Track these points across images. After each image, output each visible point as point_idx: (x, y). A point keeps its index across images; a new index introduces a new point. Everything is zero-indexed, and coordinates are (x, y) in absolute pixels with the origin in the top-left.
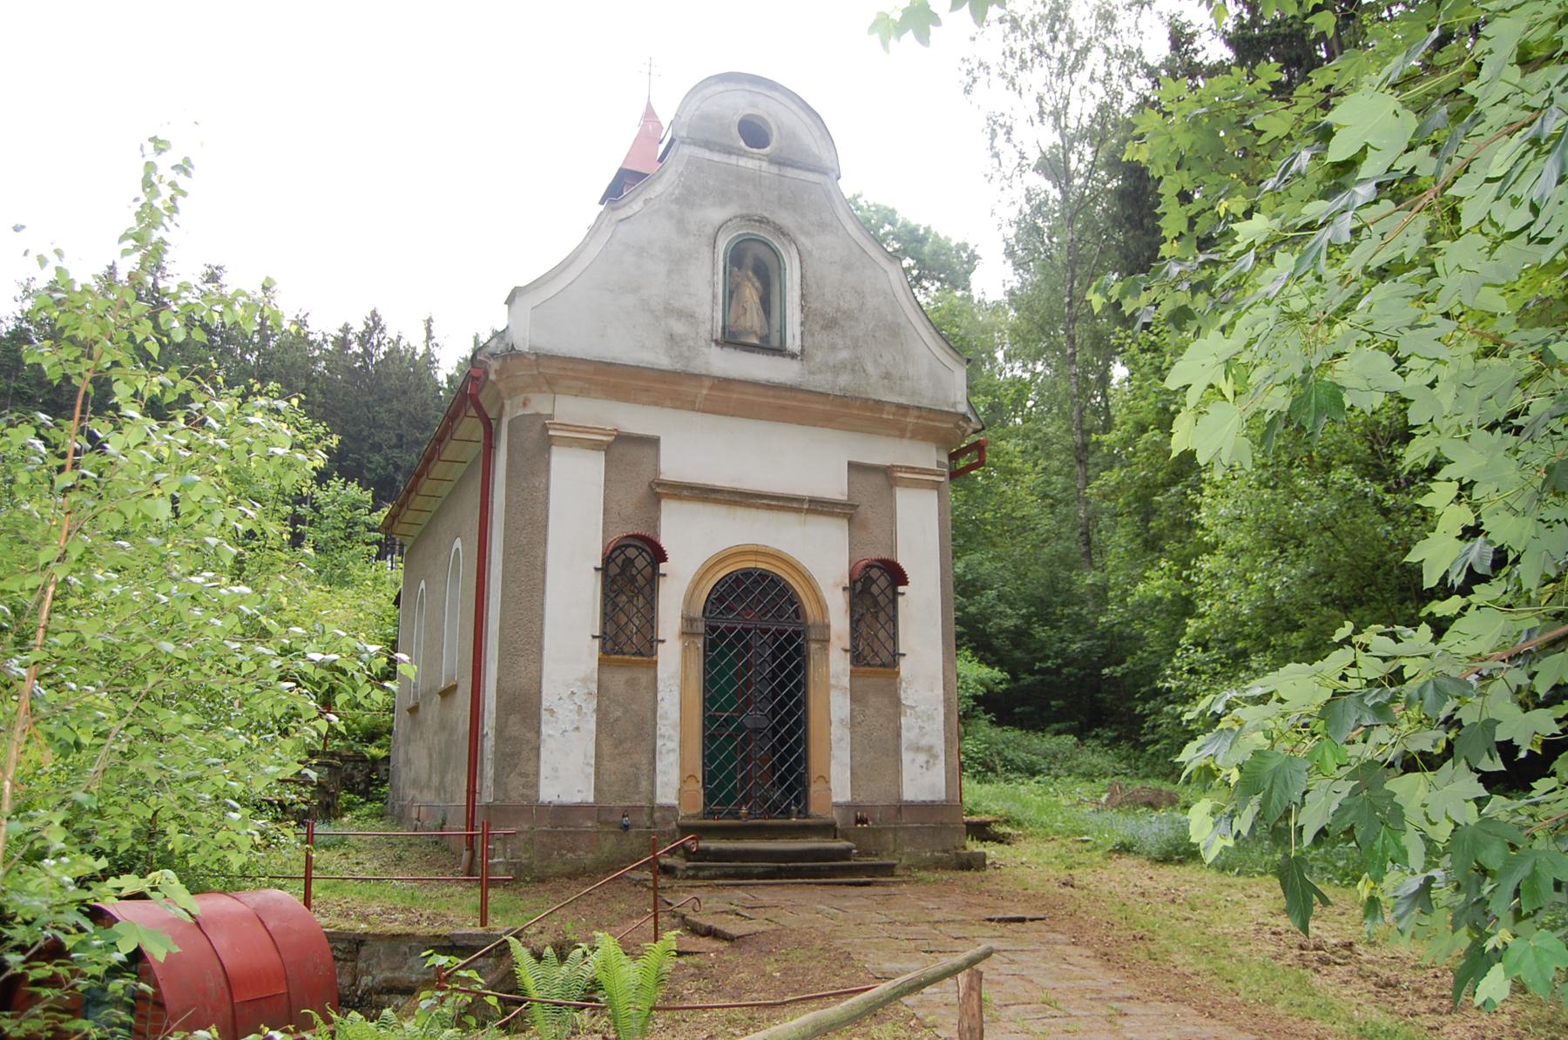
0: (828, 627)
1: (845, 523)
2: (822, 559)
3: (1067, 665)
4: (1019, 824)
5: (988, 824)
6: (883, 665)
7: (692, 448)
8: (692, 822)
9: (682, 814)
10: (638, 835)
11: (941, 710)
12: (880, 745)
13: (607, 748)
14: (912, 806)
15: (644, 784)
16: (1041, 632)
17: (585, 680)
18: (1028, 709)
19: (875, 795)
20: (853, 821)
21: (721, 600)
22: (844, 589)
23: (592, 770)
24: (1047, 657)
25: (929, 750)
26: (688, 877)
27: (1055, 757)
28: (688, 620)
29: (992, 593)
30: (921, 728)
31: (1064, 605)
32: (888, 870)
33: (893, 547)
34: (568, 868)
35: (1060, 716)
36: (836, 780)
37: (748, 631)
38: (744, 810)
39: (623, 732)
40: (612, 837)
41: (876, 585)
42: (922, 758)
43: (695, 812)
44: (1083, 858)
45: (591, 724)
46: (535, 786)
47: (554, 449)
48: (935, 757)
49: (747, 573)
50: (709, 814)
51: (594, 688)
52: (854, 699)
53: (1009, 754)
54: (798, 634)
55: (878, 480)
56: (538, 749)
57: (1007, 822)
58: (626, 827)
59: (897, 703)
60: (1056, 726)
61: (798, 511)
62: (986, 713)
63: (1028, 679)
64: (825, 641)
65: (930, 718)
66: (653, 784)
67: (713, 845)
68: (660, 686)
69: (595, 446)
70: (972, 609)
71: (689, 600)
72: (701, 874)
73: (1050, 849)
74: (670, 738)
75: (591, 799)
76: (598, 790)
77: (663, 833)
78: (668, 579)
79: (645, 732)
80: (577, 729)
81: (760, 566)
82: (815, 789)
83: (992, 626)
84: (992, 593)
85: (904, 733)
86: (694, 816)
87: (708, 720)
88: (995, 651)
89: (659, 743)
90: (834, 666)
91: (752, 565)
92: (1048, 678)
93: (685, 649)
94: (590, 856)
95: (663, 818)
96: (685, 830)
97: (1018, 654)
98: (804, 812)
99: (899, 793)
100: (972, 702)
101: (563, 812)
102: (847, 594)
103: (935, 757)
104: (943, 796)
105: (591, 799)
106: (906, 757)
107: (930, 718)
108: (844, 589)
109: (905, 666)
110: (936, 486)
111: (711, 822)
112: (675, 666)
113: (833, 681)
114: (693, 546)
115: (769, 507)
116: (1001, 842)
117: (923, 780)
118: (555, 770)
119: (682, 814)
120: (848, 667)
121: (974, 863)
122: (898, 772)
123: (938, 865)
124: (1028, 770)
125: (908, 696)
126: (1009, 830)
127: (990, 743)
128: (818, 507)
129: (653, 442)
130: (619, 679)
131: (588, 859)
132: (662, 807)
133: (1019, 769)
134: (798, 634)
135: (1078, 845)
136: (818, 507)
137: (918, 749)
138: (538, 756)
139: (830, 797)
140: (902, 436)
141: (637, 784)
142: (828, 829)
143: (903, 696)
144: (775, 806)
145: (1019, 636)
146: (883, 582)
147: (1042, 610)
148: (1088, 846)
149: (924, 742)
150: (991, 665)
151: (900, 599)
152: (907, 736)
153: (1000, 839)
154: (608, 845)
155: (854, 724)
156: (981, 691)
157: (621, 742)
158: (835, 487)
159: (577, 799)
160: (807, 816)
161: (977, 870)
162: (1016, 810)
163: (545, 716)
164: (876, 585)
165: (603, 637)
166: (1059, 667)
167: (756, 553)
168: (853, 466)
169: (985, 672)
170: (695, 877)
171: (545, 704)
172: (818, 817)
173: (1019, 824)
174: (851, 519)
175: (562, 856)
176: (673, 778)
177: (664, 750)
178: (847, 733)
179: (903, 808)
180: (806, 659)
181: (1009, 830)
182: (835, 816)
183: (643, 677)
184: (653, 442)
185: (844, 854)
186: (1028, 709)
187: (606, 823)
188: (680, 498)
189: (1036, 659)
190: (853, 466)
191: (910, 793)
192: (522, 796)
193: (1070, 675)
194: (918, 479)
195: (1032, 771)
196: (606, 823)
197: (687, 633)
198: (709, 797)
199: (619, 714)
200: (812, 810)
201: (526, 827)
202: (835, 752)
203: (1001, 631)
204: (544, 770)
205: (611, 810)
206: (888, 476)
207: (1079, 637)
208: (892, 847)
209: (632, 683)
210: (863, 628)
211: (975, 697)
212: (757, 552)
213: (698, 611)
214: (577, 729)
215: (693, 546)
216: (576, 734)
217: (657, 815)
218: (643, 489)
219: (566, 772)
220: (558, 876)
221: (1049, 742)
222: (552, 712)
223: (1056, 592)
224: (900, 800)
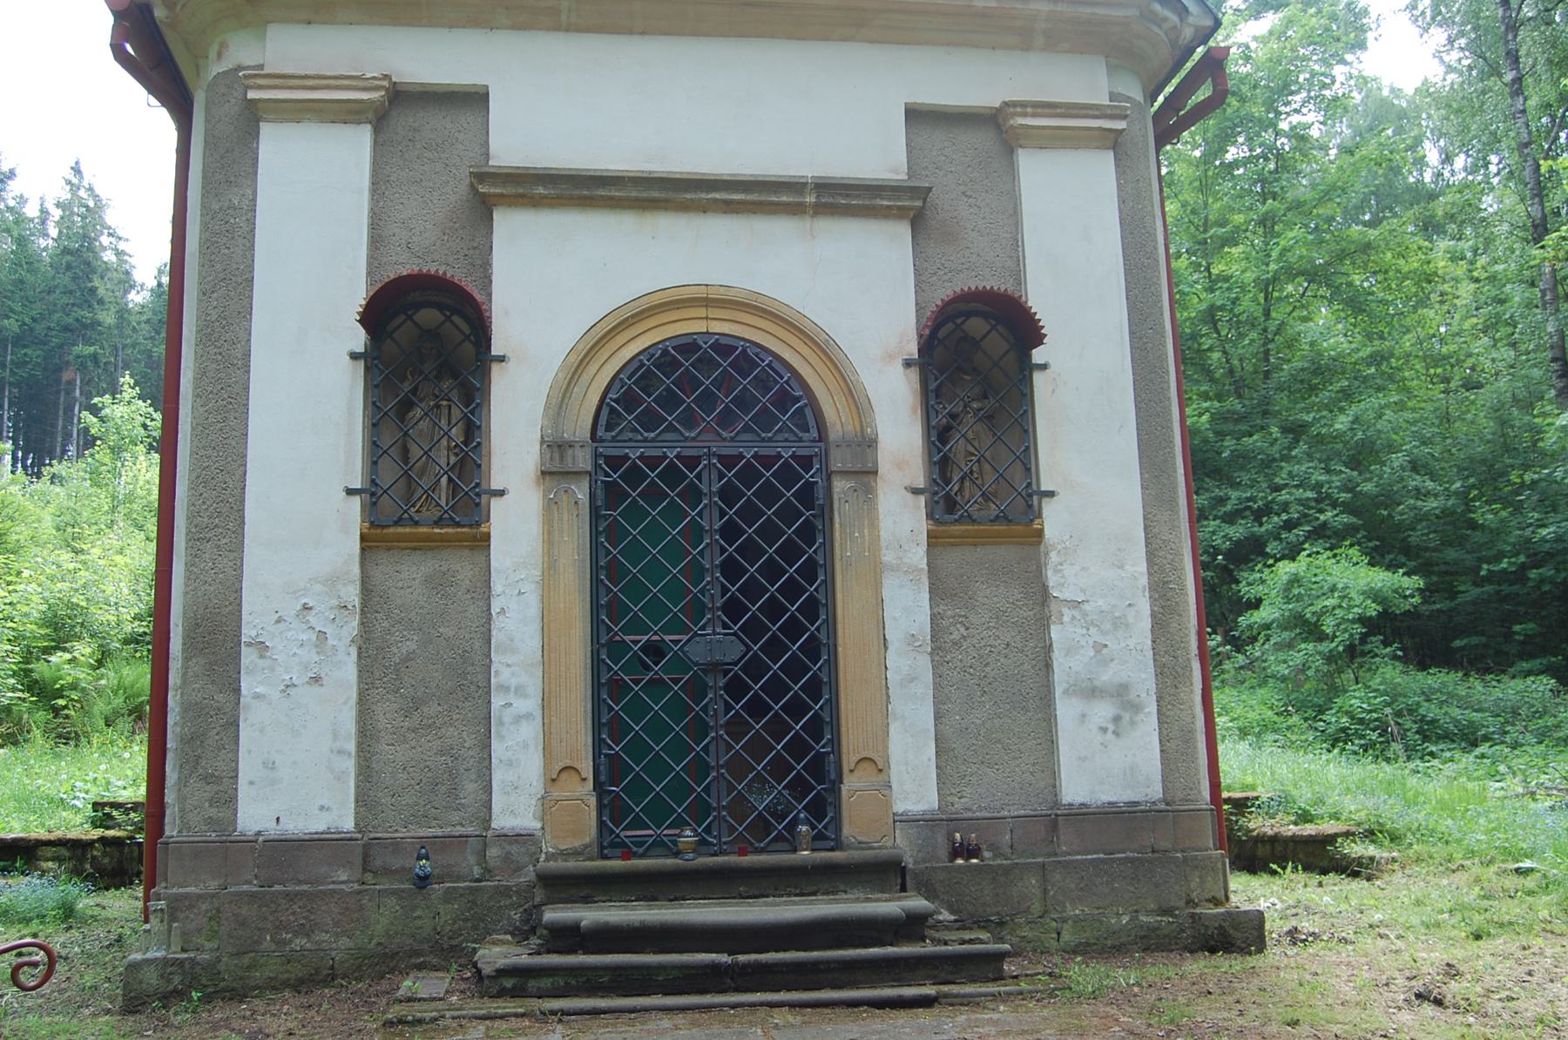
0: (871, 443)
1: (903, 230)
2: (857, 310)
3: (1537, 565)
4: (1395, 838)
5: (1331, 839)
6: (1003, 518)
7: (551, 101)
8: (572, 865)
9: (548, 847)
10: (449, 897)
11: (1144, 606)
12: (1004, 689)
13: (386, 712)
14: (1083, 816)
15: (470, 788)
16: (1485, 515)
17: (332, 581)
18: (1475, 640)
19: (995, 793)
20: (943, 852)
21: (628, 400)
22: (908, 364)
23: (350, 765)
24: (1498, 558)
25: (1121, 693)
26: (501, 994)
27: (1515, 712)
28: (555, 446)
29: (1398, 459)
30: (1099, 647)
31: (1526, 467)
32: (986, 966)
33: (1018, 274)
34: (297, 971)
35: (1530, 649)
36: (902, 761)
37: (692, 462)
38: (688, 836)
39: (418, 683)
40: (392, 901)
41: (979, 354)
42: (1103, 711)
43: (577, 843)
44: (1510, 910)
45: (348, 670)
46: (231, 801)
47: (266, 130)
48: (1136, 708)
49: (688, 346)
50: (607, 843)
51: (352, 594)
52: (938, 592)
53: (1431, 711)
54: (806, 462)
55: (979, 140)
56: (235, 724)
57: (1370, 835)
58: (423, 881)
59: (1042, 596)
60: (1525, 665)
61: (795, 210)
62: (1386, 644)
63: (1469, 592)
64: (867, 474)
65: (1119, 623)
66: (488, 789)
67: (589, 915)
68: (497, 586)
69: (347, 114)
70: (1368, 487)
71: (559, 402)
72: (532, 984)
73: (1442, 890)
74: (520, 691)
75: (348, 824)
76: (363, 800)
77: (505, 892)
78: (510, 366)
79: (469, 682)
80: (316, 680)
81: (717, 327)
82: (852, 785)
83: (1402, 512)
84: (1398, 459)
85: (1058, 658)
86: (575, 853)
87: (604, 648)
88: (1408, 550)
89: (497, 701)
90: (888, 535)
91: (700, 327)
92: (1506, 589)
93: (550, 506)
94: (344, 942)
95: (507, 858)
96: (562, 885)
97: (1451, 554)
98: (829, 835)
99: (1054, 787)
100: (1358, 629)
101: (285, 852)
102: (914, 374)
103: (1136, 708)
104: (1155, 791)
105: (348, 824)
106: (1066, 710)
107: (1119, 623)
108: (908, 364)
109: (1054, 519)
110: (1113, 141)
111: (616, 864)
112: (529, 547)
113: (888, 557)
114: (553, 304)
115: (729, 208)
116: (1355, 875)
117: (1105, 758)
118: (270, 766)
119: (548, 847)
120: (922, 525)
121: (1240, 936)
122: (1050, 744)
123: (1153, 943)
124: (1464, 737)
125: (1067, 577)
126: (1372, 850)
127: (1394, 695)
128: (837, 199)
129: (476, 99)
130: (409, 575)
131: (339, 947)
132: (503, 836)
133: (1447, 737)
134: (806, 462)
135: (1511, 882)
136: (837, 199)
137: (1092, 692)
138: (236, 739)
139: (889, 804)
140: (1026, 47)
141: (454, 791)
142: (886, 872)
143: (1052, 579)
144: (761, 827)
145: (1457, 524)
146: (997, 344)
147: (1488, 475)
148: (1530, 882)
149: (1106, 677)
150: (1392, 567)
151: (1038, 377)
152: (1065, 666)
153: (1353, 869)
154: (384, 920)
155: (940, 643)
156: (1373, 609)
157: (417, 704)
158: (879, 153)
159: (314, 823)
160: (838, 845)
161: (1244, 951)
162: (1390, 812)
163: (248, 657)
164: (979, 354)
165: (371, 494)
166: (1523, 568)
167: (706, 302)
168: (916, 116)
169: (1380, 578)
170: (517, 993)
171: (247, 633)
172: (861, 845)
173: (1395, 838)
174: (917, 221)
175: (282, 943)
176: (529, 773)
177: (508, 716)
178: (924, 665)
179: (1060, 821)
180: (826, 512)
181: (1372, 850)
182: (903, 845)
183: (461, 566)
184: (476, 99)
185: (912, 927)
186: (1475, 640)
187: (387, 872)
188: (535, 203)
189: (1481, 560)
190: (916, 116)
191: (1076, 788)
192: (210, 821)
193: (1542, 581)
194: (1069, 129)
195: (1469, 738)
196: (387, 872)
197: (553, 473)
198: (611, 809)
199: (412, 646)
200: (850, 830)
201: (213, 885)
202: (898, 705)
203: (1422, 517)
204: (248, 768)
205: (396, 846)
206: (1000, 130)
207: (1552, 517)
208: (1037, 907)
209: (439, 583)
210: (958, 445)
211: (1362, 620)
212: (708, 301)
213: (580, 423)
214: (316, 680)
215: (553, 304)
216: (316, 689)
217: (493, 852)
218: (456, 190)
219: (296, 770)
220: (275, 985)
221: (1510, 689)
222: (262, 648)
223: (1508, 449)
224: (1056, 804)
